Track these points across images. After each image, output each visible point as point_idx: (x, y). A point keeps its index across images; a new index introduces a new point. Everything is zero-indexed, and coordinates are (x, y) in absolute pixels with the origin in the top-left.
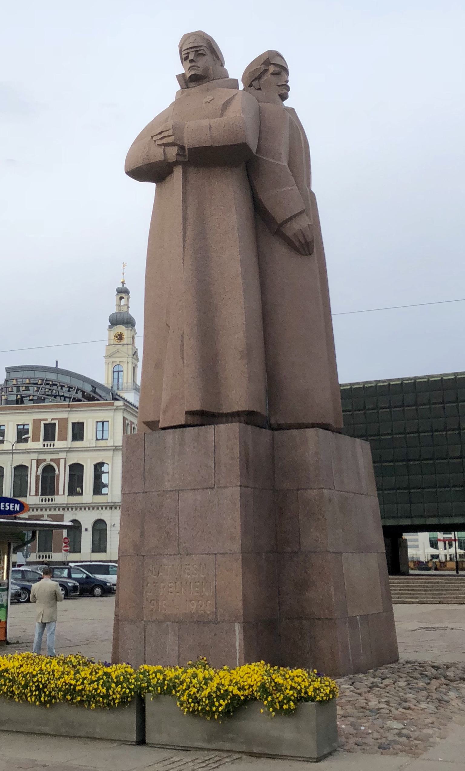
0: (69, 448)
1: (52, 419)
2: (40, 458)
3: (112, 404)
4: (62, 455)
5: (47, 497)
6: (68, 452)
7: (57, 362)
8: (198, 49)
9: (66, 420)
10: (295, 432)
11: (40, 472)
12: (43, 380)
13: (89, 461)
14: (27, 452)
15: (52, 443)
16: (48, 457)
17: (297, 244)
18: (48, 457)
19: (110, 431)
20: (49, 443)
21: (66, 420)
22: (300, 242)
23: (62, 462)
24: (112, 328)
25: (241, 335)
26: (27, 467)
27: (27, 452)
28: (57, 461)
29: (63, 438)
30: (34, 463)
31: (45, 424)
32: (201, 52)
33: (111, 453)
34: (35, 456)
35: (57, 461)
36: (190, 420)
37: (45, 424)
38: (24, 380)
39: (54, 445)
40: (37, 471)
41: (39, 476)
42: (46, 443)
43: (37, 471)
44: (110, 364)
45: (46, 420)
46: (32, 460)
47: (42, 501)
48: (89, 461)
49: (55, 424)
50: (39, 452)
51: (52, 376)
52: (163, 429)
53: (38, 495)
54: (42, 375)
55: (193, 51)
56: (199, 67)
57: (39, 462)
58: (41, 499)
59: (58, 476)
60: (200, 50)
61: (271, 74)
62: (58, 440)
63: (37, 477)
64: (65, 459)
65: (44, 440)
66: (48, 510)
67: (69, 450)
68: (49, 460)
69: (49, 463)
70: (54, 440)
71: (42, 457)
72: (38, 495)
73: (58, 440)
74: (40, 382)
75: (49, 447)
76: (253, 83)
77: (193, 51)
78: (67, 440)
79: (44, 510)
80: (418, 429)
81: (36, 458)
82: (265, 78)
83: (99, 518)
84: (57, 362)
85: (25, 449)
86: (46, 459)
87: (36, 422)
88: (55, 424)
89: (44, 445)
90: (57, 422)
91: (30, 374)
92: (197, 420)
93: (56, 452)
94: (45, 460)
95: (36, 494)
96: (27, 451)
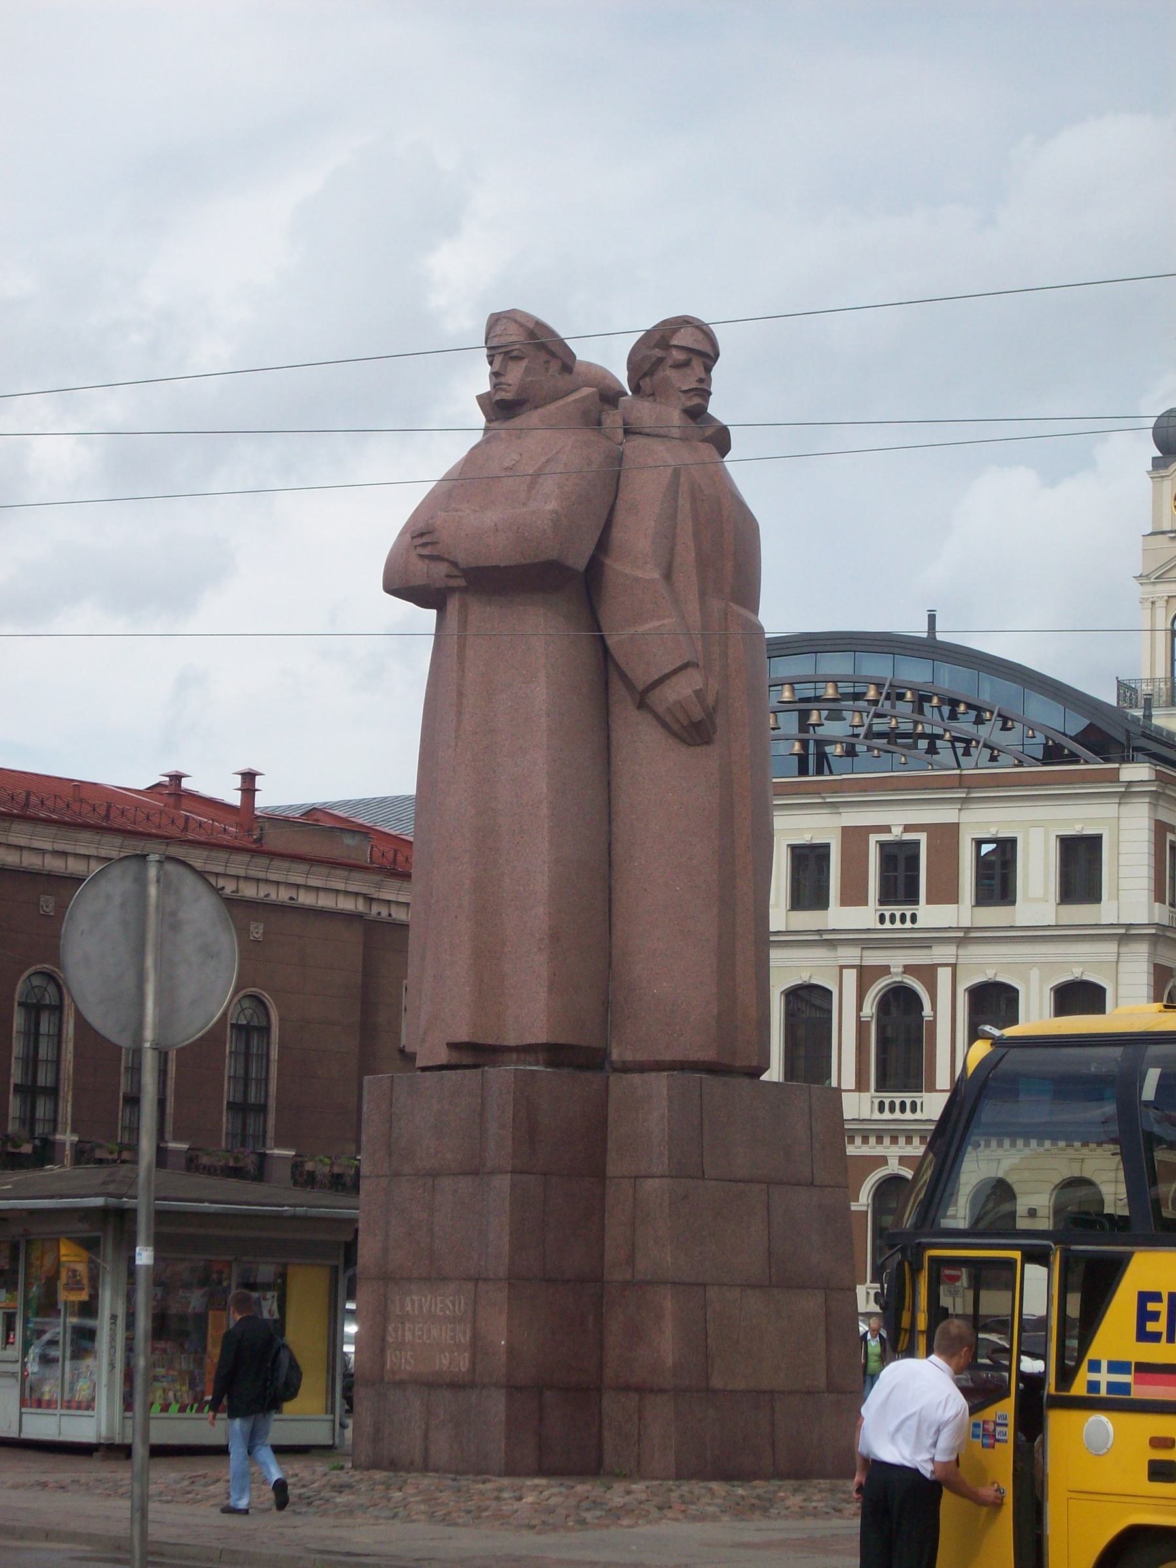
0: (968, 929)
1: (908, 828)
2: (867, 962)
3: (1113, 776)
4: (941, 954)
5: (897, 1097)
6: (961, 942)
7: (932, 619)
8: (509, 349)
9: (953, 829)
10: (636, 1078)
11: (869, 1009)
12: (879, 686)
13: (1035, 974)
14: (827, 940)
15: (908, 910)
16: (897, 960)
17: (675, 727)
18: (897, 960)
19: (120, 1127)
20: (897, 910)
21: (953, 829)
22: (678, 721)
23: (944, 975)
24: (1166, 467)
25: (541, 911)
26: (829, 993)
27: (827, 940)
28: (927, 974)
29: (946, 893)
30: (850, 977)
31: (882, 845)
32: (515, 354)
33: (1111, 948)
34: (851, 955)
35: (927, 974)
36: (455, 1058)
37: (882, 845)
38: (819, 685)
39: (914, 918)
40: (860, 1007)
41: (868, 1023)
42: (888, 910)
43: (860, 1007)
44: (1161, 603)
45: (887, 829)
46: (842, 967)
47: (881, 1108)
48: (1035, 974)
49: (917, 843)
50: (865, 940)
51: (915, 673)
52: (424, 1069)
53: (868, 1090)
54: (878, 667)
55: (500, 353)
56: (509, 385)
57: (866, 976)
58: (877, 1101)
59: (933, 1024)
60: (512, 350)
61: (670, 366)
62: (929, 902)
63: (862, 1027)
64: (954, 966)
65: (882, 902)
66: (902, 1140)
67: (965, 937)
68: (900, 970)
69: (899, 979)
70: (917, 902)
71: (874, 958)
72: (868, 1090)
73: (929, 902)
74: (872, 694)
75: (898, 925)
76: (641, 383)
77: (500, 353)
78: (957, 903)
79: (887, 1140)
80: (633, 1276)
81: (857, 962)
82: (660, 374)
83: (1077, 1174)
84: (932, 619)
85: (819, 932)
86: (888, 967)
87: (854, 837)
88: (917, 843)
89: (882, 919)
90: (922, 837)
91: (837, 664)
92: (467, 1060)
93: (924, 944)
94: (885, 970)
95: (861, 1086)
96: (825, 937)
